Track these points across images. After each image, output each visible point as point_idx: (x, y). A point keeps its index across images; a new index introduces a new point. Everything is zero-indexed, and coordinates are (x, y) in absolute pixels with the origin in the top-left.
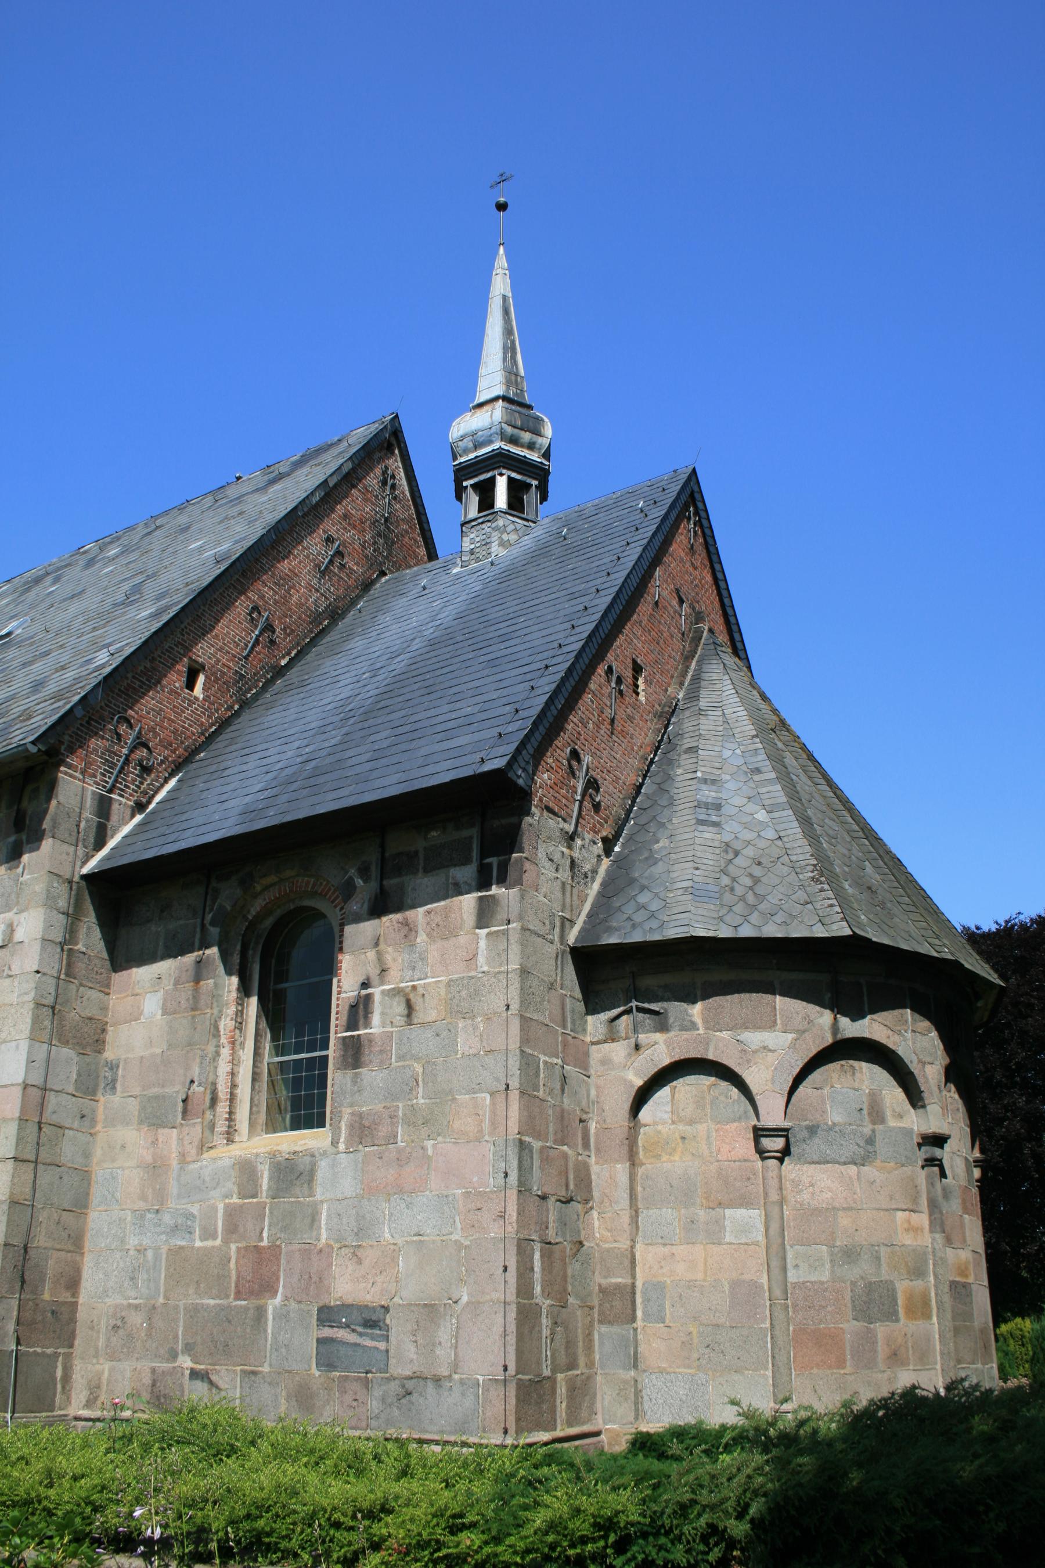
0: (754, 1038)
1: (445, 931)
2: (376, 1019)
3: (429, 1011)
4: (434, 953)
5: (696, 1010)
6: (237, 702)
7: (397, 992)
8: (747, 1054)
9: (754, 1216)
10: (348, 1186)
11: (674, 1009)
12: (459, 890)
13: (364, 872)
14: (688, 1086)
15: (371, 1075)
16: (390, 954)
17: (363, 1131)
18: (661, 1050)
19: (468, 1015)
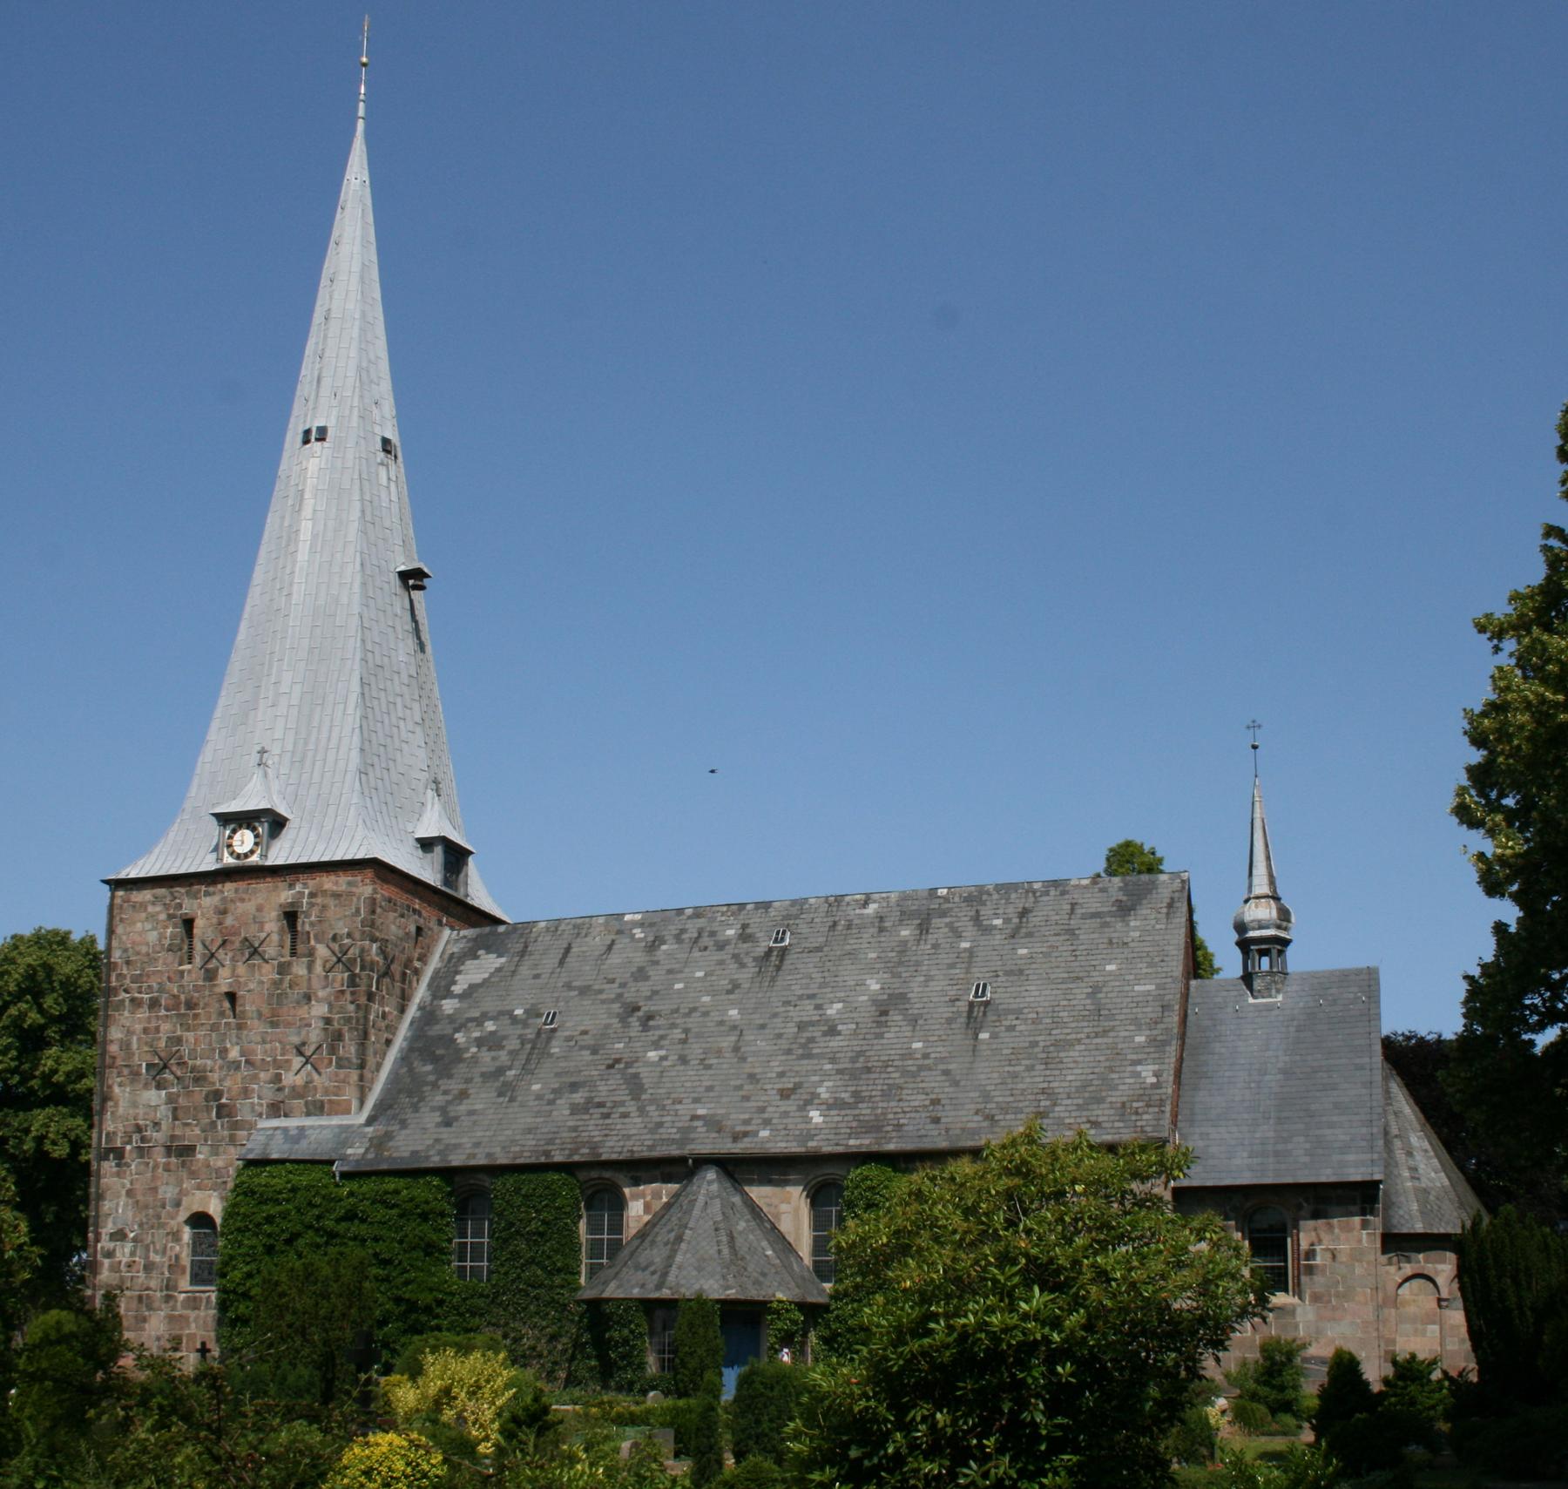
0: (1440, 1267)
1: (1349, 1229)
2: (1318, 1258)
3: (1342, 1258)
4: (1343, 1236)
5: (1421, 1256)
6: (90, 1422)
7: (1327, 1250)
8: (1437, 1272)
9: (1436, 1327)
10: (1311, 1316)
11: (1413, 1255)
12: (1353, 1215)
13: (1307, 1201)
14: (1416, 1283)
15: (1318, 1279)
16: (1323, 1235)
17: (1316, 1298)
18: (1408, 1269)
19: (1360, 1261)
